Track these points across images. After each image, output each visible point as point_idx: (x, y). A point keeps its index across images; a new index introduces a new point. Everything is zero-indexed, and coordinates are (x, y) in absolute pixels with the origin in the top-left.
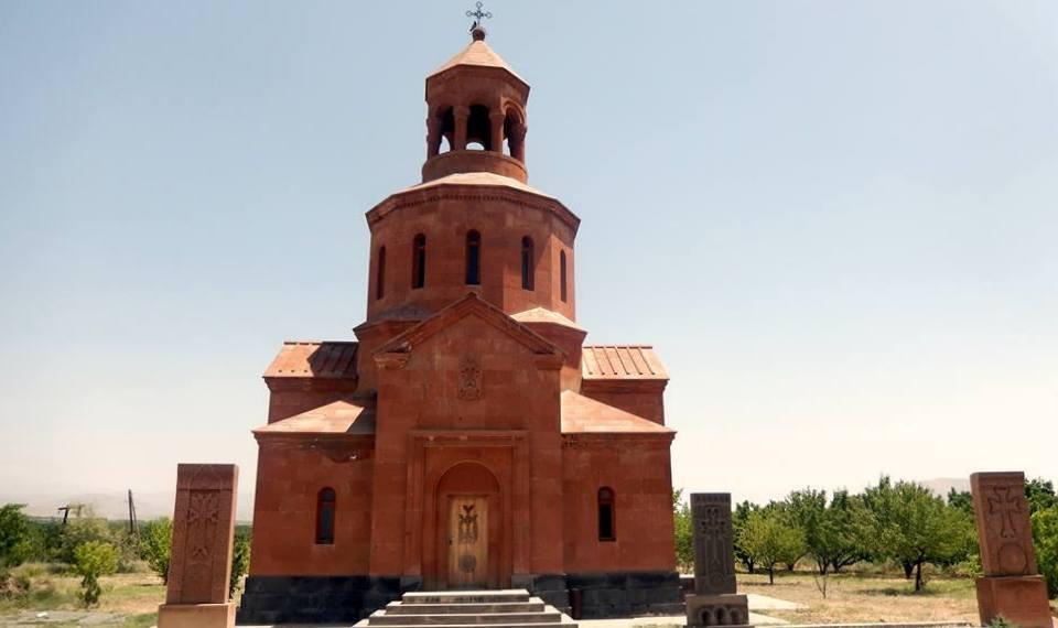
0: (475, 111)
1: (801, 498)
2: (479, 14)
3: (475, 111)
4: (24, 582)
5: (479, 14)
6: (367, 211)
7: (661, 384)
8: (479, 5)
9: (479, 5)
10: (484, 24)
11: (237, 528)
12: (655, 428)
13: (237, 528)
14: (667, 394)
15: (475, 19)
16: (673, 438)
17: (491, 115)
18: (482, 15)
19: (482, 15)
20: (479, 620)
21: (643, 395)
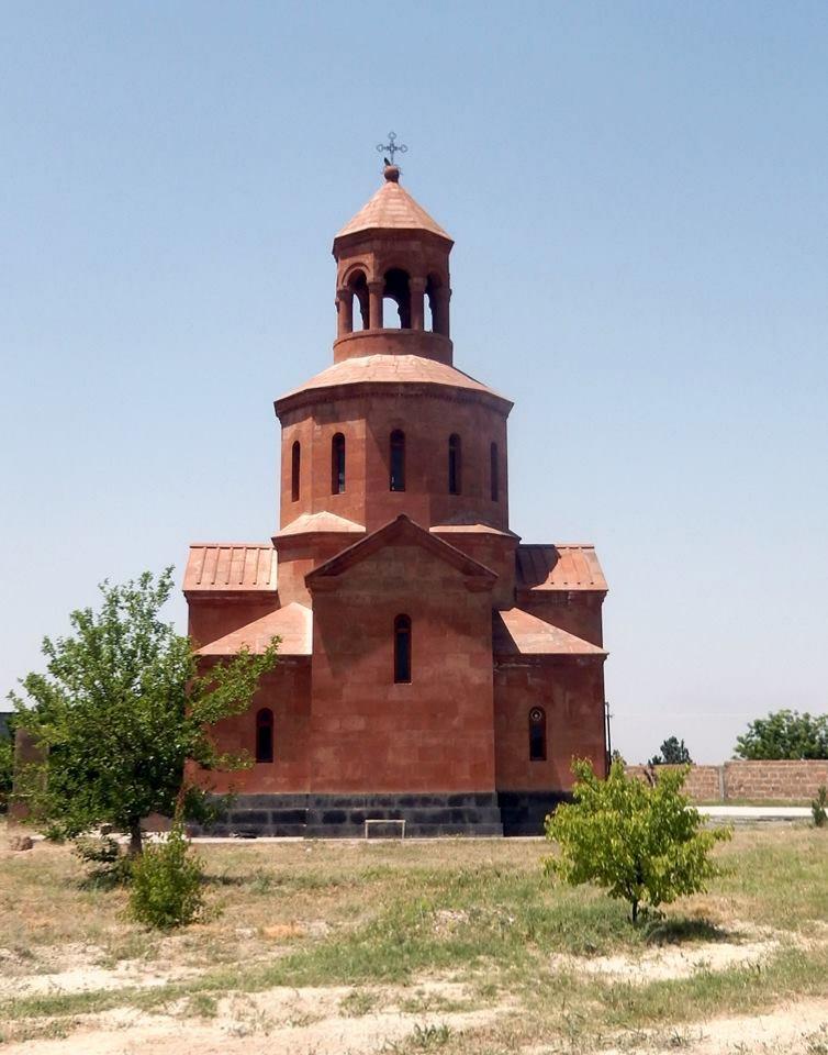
0: (399, 274)
1: (35, 822)
2: (392, 148)
3: (399, 274)
4: (580, 916)
5: (392, 148)
6: (337, 236)
7: (598, 596)
8: (392, 136)
9: (392, 136)
10: (399, 161)
11: (348, 343)
12: (596, 650)
13: (348, 343)
14: (606, 607)
15: (387, 154)
16: (606, 658)
17: (410, 281)
18: (396, 148)
19: (396, 148)
20: (386, 815)
21: (583, 610)
